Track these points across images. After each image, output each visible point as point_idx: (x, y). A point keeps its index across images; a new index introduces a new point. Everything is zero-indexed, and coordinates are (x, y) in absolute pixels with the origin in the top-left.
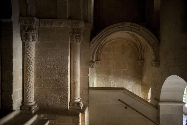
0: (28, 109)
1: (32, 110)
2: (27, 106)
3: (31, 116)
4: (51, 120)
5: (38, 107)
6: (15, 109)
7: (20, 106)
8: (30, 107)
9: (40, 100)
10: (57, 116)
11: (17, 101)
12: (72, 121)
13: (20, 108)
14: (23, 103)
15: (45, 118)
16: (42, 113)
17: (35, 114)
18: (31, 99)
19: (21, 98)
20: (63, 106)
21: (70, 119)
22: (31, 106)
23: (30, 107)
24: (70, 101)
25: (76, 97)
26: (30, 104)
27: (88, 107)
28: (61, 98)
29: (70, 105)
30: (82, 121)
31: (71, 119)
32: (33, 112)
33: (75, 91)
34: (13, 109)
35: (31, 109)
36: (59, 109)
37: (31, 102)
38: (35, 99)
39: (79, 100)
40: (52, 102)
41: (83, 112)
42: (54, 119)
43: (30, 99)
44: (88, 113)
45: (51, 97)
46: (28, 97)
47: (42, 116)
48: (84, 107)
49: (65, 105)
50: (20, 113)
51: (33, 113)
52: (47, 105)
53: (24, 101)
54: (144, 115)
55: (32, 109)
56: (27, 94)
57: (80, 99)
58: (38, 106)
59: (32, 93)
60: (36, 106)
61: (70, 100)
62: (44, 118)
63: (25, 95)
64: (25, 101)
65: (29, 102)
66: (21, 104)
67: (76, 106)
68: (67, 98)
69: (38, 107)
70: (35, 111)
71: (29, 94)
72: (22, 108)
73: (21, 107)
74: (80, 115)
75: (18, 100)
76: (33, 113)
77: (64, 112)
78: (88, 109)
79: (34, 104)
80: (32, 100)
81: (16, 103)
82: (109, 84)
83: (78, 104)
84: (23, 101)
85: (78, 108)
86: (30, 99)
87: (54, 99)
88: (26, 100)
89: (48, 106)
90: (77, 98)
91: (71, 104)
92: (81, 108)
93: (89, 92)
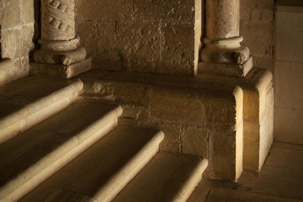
0: (51, 60)
1: (67, 66)
2: (51, 51)
3: (59, 83)
4: (128, 103)
5: (90, 59)
6: (12, 57)
7: (28, 50)
8: (60, 57)
9: (94, 37)
10: (150, 93)
11: (17, 32)
12: (207, 112)
13: (28, 57)
14: (40, 42)
15: (109, 97)
16: (101, 79)
17: (74, 79)
18: (64, 28)
19: (31, 25)
20: (176, 60)
21: (200, 106)
22: (64, 52)
23: (60, 57)
24: (203, 47)
25: (226, 32)
26: (60, 47)
27: (273, 73)
28: (167, 30)
29: (200, 60)
30: (245, 120)
31: (203, 105)
32: (70, 72)
33: (222, 7)
34: (4, 56)
35: (61, 63)
36: (162, 71)
37: (65, 41)
38: (78, 34)
39: (235, 44)
40: (137, 46)
41: (251, 87)
42: (139, 104)
43: (59, 27)
44: (271, 94)
45: (132, 26)
46: (54, 19)
47: (98, 88)
48: (256, 73)
49: (183, 55)
50: (30, 75)
51: (69, 75)
52: (120, 55)
53: (42, 36)
54: (287, 143)
55: (64, 63)
56: (48, 11)
57: (241, 40)
58: (87, 58)
59: (64, 7)
60: (82, 55)
61: (202, 39)
62: (106, 94)
63: (43, 15)
64: (43, 35)
65: (55, 39)
66: (32, 45)
67: (225, 63)
68: (191, 30)
69: (90, 59)
70: (75, 70)
71: (57, 12)
72: (36, 59)
73: (31, 54)
74: (240, 96)
75: (19, 27)
76: (69, 75)
77: (180, 81)
78: (273, 81)
79: (75, 46)
80: (67, 33)
81: (12, 36)
82: (253, 79)
83: (234, 55)
84: (40, 37)
85: (230, 70)
86: (59, 27)
87: (142, 31)
88: (49, 32)
89: (122, 59)
90: (228, 36)
91: (204, 58)
92: (241, 71)
93: (278, 14)
